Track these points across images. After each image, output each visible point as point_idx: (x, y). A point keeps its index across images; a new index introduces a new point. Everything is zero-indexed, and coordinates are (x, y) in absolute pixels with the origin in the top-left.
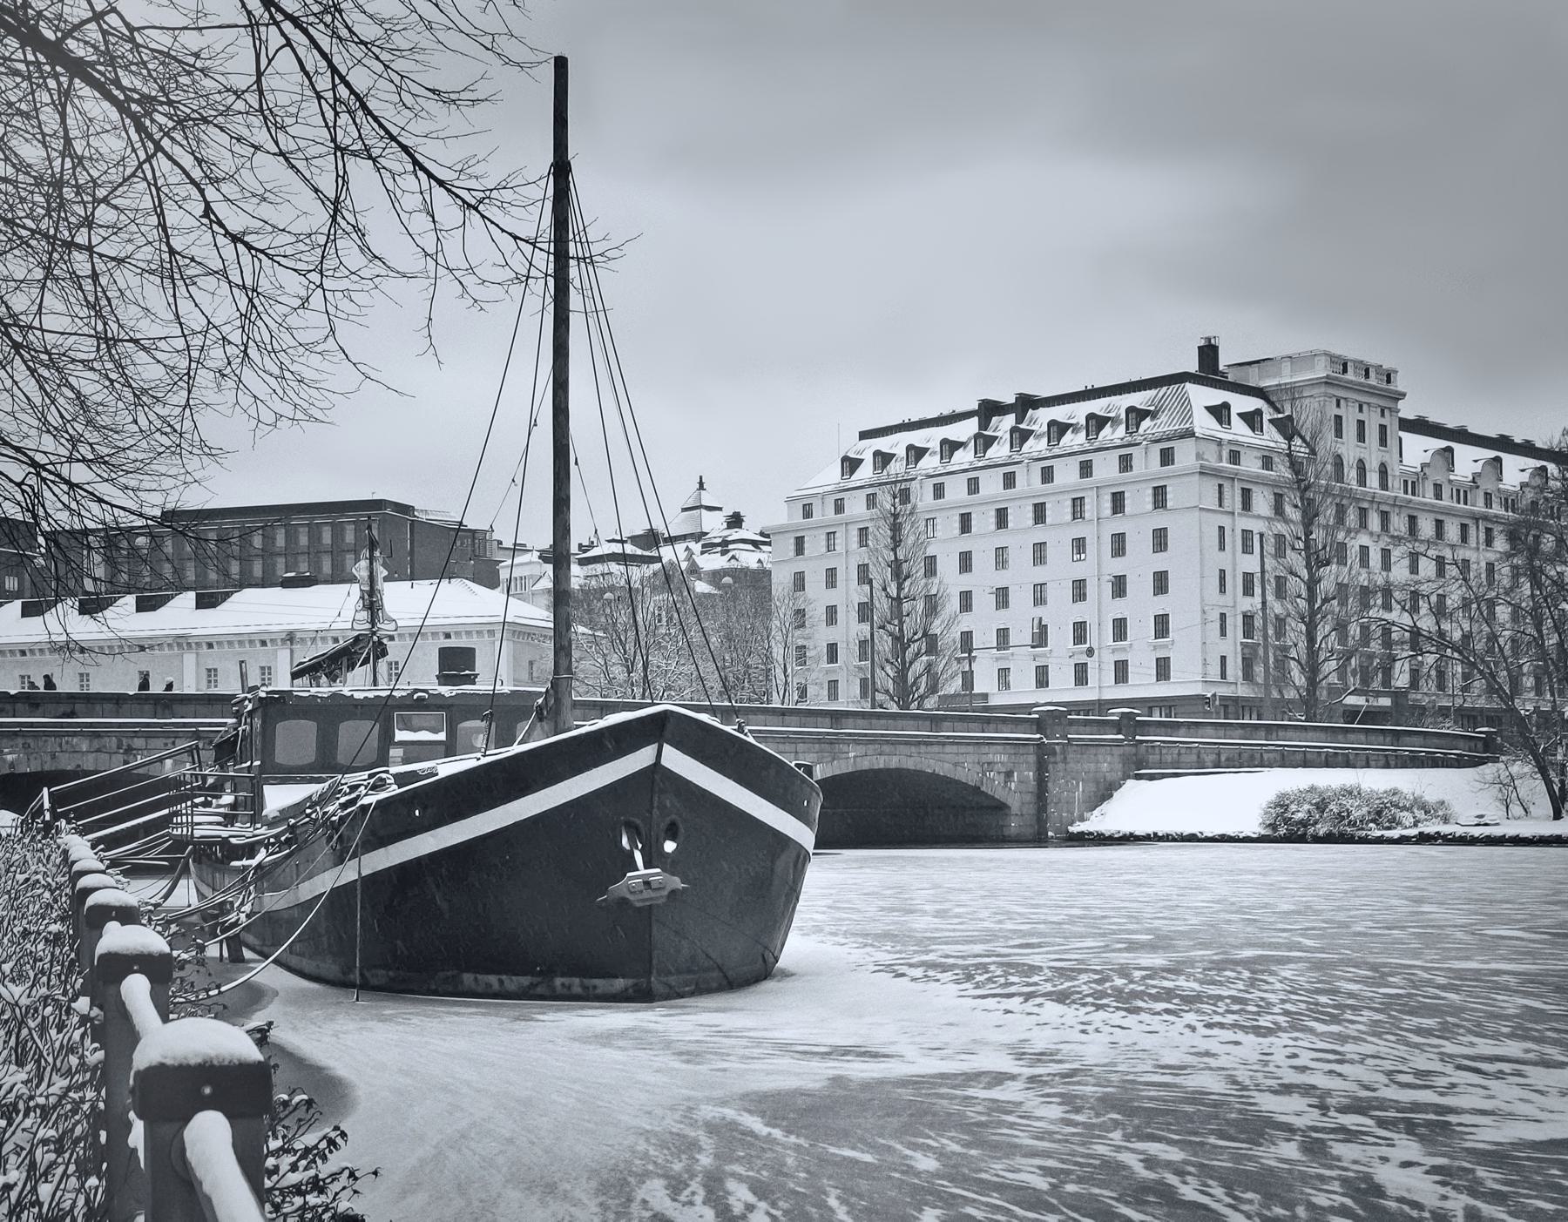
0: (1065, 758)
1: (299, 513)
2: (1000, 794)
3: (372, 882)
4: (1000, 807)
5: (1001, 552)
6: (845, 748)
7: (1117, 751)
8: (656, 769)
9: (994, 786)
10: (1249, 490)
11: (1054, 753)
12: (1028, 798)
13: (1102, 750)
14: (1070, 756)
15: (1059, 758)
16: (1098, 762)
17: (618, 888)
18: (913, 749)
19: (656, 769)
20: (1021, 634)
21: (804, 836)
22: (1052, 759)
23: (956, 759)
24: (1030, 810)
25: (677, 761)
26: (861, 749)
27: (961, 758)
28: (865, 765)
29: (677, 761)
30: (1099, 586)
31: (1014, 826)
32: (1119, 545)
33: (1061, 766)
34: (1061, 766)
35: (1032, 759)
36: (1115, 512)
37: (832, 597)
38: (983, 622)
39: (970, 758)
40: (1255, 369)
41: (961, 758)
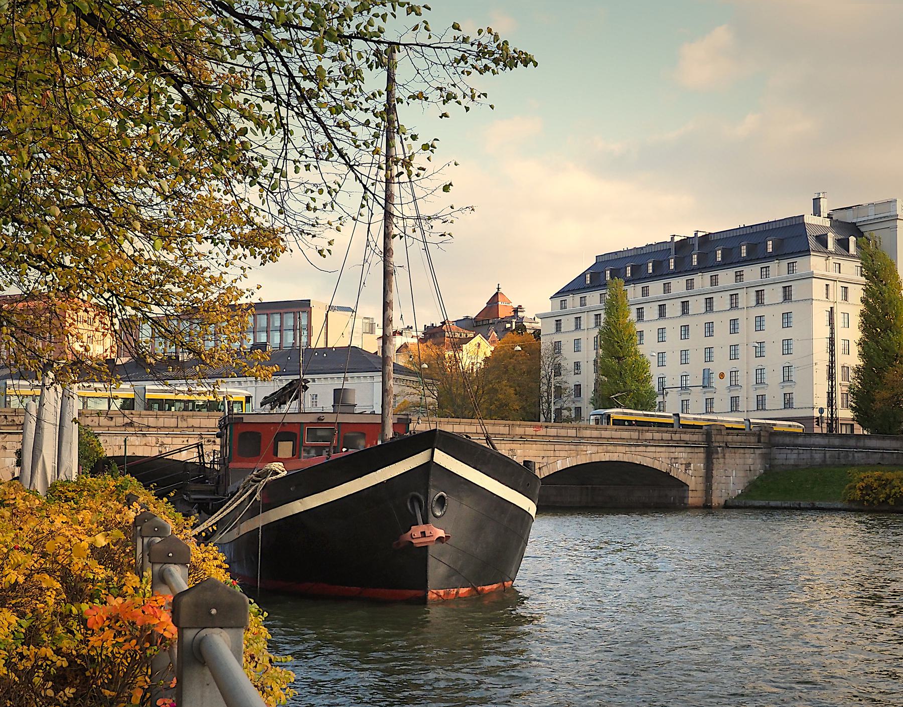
0: (724, 455)
1: (287, 307)
2: (682, 477)
3: (267, 527)
4: (683, 486)
5: (662, 331)
6: (584, 448)
7: (758, 451)
8: (430, 465)
9: (678, 473)
10: (846, 288)
11: (718, 453)
12: (700, 480)
13: (747, 451)
14: (727, 455)
15: (720, 455)
16: (744, 458)
17: (407, 537)
18: (627, 449)
19: (430, 465)
20: (695, 379)
21: (528, 505)
22: (716, 456)
23: (654, 455)
24: (701, 487)
25: (442, 458)
26: (595, 449)
27: (658, 455)
28: (596, 458)
29: (442, 458)
30: (747, 349)
31: (694, 497)
32: (709, 329)
33: (721, 460)
34: (721, 460)
35: (702, 456)
36: (785, 300)
37: (577, 357)
38: (672, 372)
39: (662, 455)
40: (850, 211)
41: (658, 455)
